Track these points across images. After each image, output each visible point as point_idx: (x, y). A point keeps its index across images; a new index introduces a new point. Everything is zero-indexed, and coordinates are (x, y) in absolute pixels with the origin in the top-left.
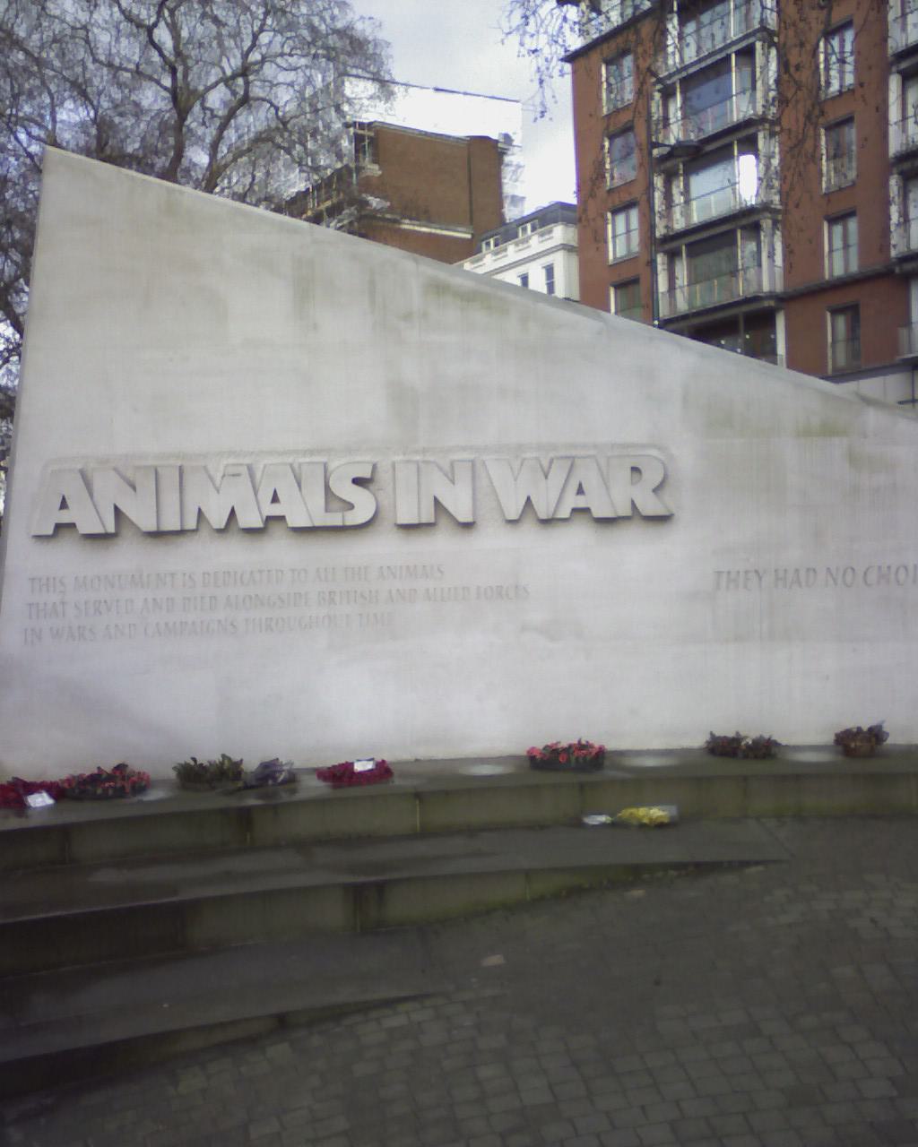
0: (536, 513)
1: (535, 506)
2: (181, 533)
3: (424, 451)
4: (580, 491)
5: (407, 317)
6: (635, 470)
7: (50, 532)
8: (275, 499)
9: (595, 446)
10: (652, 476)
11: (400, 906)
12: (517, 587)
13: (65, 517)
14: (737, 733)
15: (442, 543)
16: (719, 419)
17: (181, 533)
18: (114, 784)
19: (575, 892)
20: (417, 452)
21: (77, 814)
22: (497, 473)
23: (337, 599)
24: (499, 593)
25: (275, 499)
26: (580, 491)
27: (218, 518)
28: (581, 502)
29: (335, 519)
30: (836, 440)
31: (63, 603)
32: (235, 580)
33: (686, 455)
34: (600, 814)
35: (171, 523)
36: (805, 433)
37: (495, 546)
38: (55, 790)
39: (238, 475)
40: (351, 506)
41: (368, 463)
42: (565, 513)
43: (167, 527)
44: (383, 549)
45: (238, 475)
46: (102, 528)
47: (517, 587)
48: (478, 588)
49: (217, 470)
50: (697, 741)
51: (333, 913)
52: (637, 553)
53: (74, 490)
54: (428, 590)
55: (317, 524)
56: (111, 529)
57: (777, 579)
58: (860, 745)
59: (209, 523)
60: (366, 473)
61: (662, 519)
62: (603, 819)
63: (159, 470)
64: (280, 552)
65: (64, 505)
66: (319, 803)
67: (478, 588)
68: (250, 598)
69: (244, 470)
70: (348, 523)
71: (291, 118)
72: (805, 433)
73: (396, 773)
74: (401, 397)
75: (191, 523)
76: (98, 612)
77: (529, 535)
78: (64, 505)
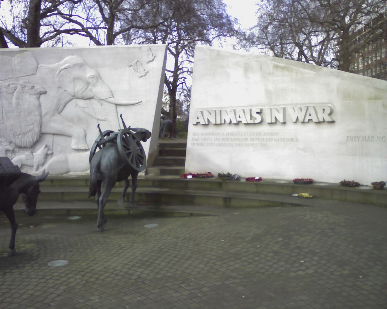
0: (279, 122)
1: (279, 120)
2: (221, 124)
3: (274, 105)
4: (310, 115)
5: (269, 74)
6: (324, 110)
7: (195, 123)
8: (240, 117)
9: (315, 103)
10: (328, 111)
11: (234, 203)
12: (296, 138)
13: (198, 121)
14: (344, 180)
15: (278, 128)
16: (346, 96)
17: (221, 124)
18: (208, 175)
19: (269, 206)
20: (272, 106)
21: (195, 179)
22: (290, 110)
23: (254, 140)
24: (292, 140)
25: (240, 117)
26: (310, 115)
27: (228, 121)
28: (310, 118)
29: (252, 122)
30: (379, 101)
31: (199, 138)
32: (271, 134)
33: (338, 106)
34: (296, 194)
35: (218, 122)
36: (370, 99)
37: (291, 127)
38: (194, 176)
39: (231, 112)
40: (256, 119)
41: (259, 109)
42: (306, 120)
43: (273, 122)
44: (265, 128)
45: (231, 112)
46: (204, 122)
47: (296, 138)
48: (287, 138)
49: (228, 110)
50: (338, 181)
51: (221, 202)
52: (326, 130)
53: (200, 115)
54: (275, 139)
55: (249, 122)
56: (207, 123)
57: (364, 139)
58: (379, 186)
59: (211, 123)
60: (259, 111)
61: (333, 122)
62: (297, 195)
63: (216, 111)
64: (242, 129)
65: (198, 118)
66: (243, 183)
67: (287, 138)
68: (236, 139)
69: (233, 111)
70: (255, 122)
71: (311, 8)
72: (370, 99)
73: (262, 180)
74: (268, 93)
75: (223, 122)
76: (205, 140)
77: (299, 126)
78: (198, 118)
